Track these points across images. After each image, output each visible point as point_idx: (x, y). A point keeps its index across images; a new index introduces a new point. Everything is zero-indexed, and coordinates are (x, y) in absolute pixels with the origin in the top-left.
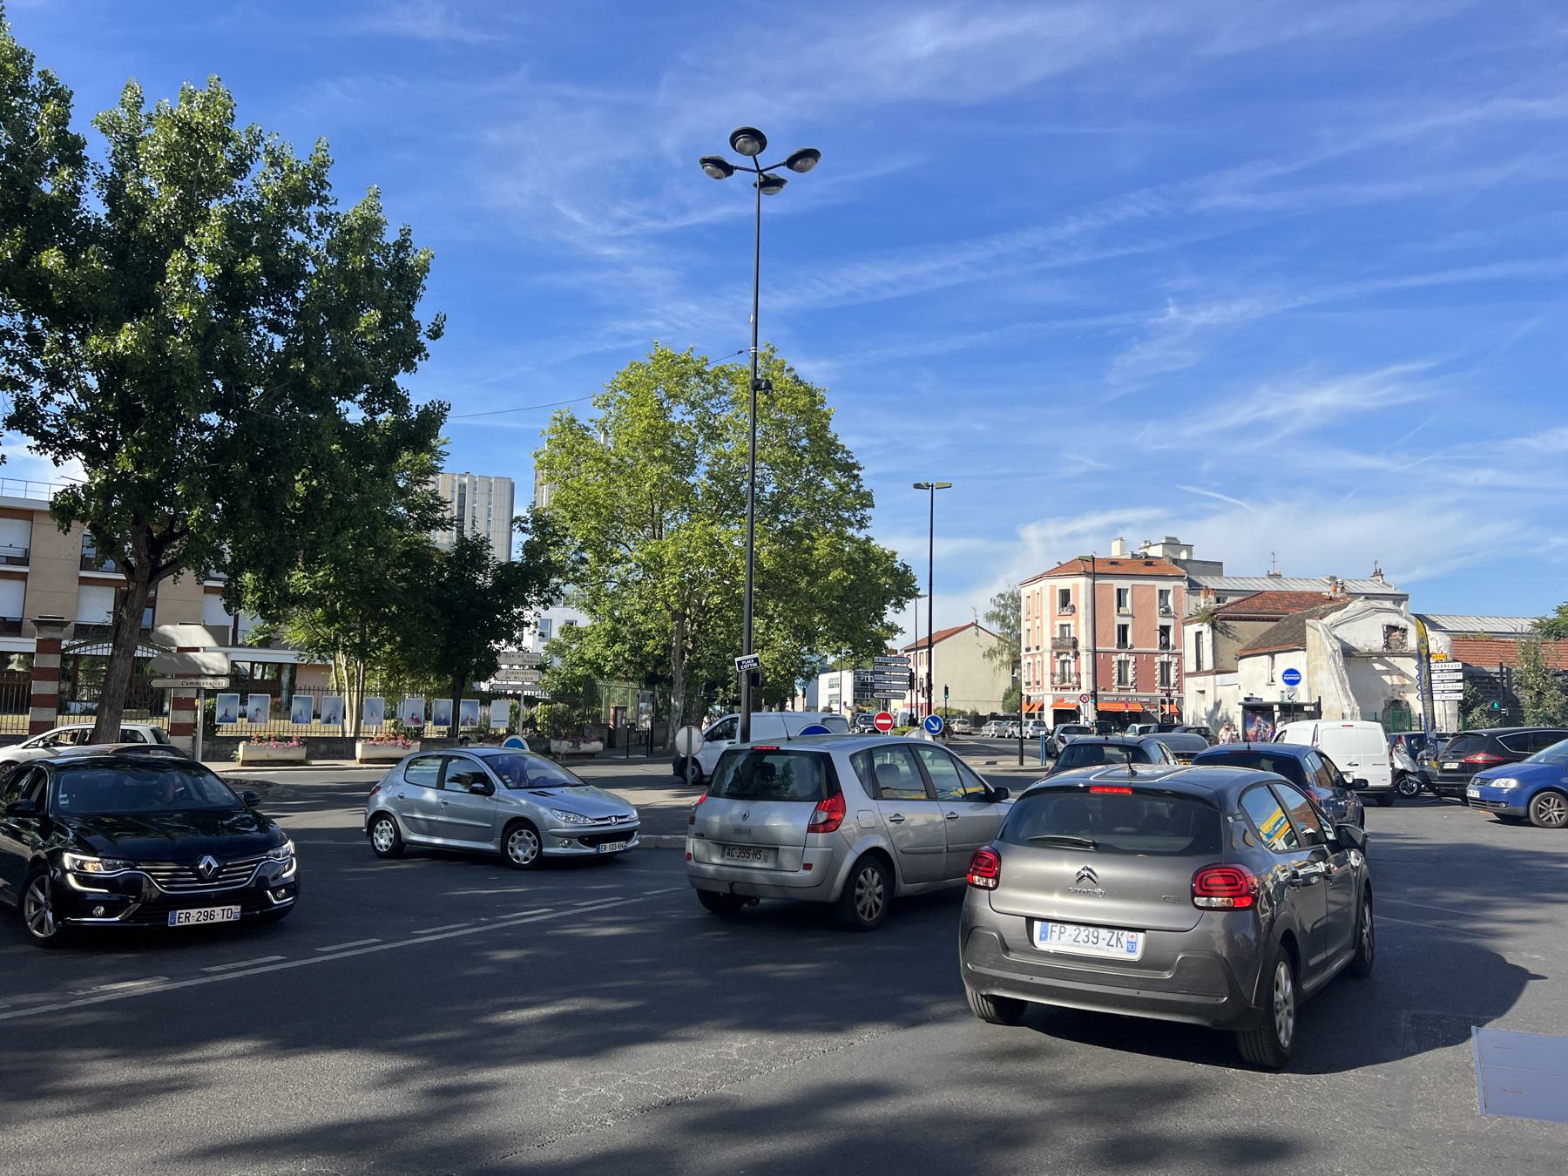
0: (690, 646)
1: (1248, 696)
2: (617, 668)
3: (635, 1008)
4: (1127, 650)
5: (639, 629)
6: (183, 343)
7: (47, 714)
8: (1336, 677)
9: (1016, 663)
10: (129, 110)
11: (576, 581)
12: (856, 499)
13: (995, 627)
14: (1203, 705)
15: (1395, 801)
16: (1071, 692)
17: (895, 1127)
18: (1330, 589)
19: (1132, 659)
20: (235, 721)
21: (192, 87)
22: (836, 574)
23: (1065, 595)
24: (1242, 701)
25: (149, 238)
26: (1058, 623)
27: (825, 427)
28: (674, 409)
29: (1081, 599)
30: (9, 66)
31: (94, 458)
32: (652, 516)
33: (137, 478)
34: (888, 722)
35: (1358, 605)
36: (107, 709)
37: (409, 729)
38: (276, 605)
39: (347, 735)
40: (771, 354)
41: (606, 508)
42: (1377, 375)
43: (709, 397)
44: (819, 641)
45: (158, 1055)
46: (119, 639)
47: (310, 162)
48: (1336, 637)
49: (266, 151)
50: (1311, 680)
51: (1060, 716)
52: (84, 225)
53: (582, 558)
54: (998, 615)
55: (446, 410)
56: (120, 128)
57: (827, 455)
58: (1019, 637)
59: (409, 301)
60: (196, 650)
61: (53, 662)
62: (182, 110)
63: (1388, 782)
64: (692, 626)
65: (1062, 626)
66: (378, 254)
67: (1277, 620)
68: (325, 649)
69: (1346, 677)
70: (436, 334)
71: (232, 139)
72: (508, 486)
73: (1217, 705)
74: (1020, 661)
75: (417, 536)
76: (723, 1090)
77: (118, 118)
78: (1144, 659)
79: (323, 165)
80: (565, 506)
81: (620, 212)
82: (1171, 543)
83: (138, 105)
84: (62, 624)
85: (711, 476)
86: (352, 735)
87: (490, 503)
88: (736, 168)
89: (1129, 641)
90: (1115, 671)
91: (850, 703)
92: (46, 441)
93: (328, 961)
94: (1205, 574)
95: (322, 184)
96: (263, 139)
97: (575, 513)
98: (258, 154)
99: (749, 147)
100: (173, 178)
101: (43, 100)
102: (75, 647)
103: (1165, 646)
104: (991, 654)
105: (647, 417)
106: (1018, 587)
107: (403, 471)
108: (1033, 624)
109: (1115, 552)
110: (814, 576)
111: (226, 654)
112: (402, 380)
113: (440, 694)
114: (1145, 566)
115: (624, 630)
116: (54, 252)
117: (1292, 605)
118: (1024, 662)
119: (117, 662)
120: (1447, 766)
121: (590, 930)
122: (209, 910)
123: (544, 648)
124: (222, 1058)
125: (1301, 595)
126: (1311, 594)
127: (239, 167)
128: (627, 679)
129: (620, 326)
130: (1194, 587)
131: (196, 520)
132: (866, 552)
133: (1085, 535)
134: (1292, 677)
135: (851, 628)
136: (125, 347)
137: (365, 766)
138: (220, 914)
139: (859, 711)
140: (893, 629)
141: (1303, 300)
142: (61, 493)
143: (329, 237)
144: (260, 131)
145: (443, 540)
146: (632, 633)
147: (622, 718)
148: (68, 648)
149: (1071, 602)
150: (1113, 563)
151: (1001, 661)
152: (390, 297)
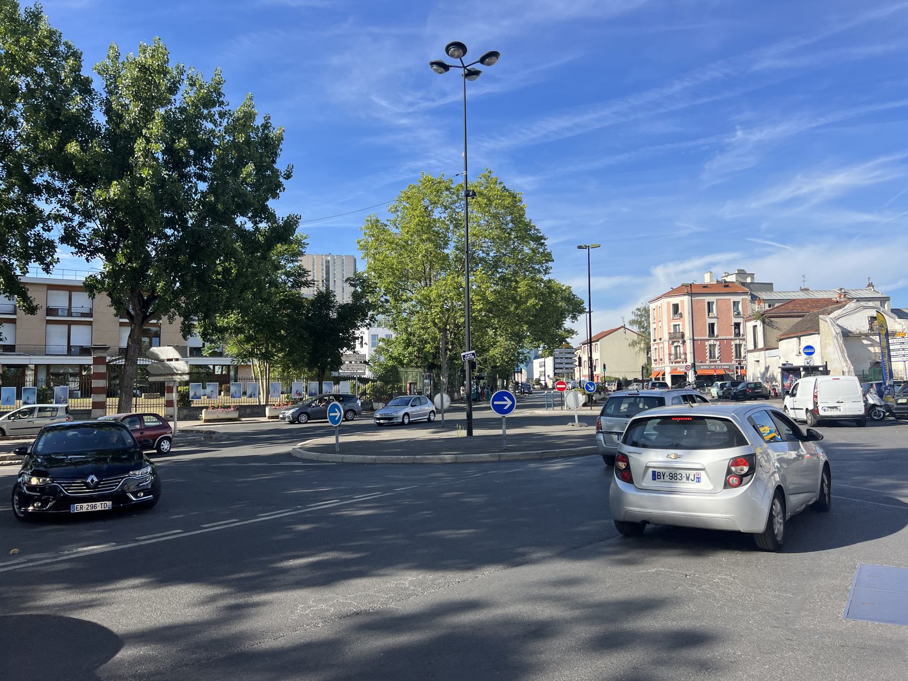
0: (450, 347)
1: (785, 363)
2: (411, 361)
3: (362, 558)
4: (714, 338)
5: (423, 338)
6: (146, 191)
7: (101, 398)
8: (838, 349)
9: (648, 349)
10: (112, 61)
11: (383, 313)
12: (542, 257)
13: (635, 328)
14: (759, 369)
15: (867, 423)
16: (681, 364)
17: (481, 626)
18: (837, 296)
19: (718, 343)
20: (200, 398)
21: (145, 44)
22: (532, 301)
23: (676, 307)
24: (781, 366)
25: (125, 131)
26: (672, 324)
27: (522, 216)
28: (435, 210)
29: (685, 309)
30: (46, 41)
31: (110, 257)
32: (424, 273)
33: (129, 267)
34: (564, 386)
35: (852, 305)
36: (124, 394)
37: (295, 399)
38: (211, 332)
39: (262, 404)
40: (489, 174)
41: (398, 270)
42: (871, 164)
43: (454, 202)
44: (526, 341)
45: (92, 587)
46: (128, 357)
47: (211, 82)
48: (838, 325)
49: (188, 78)
50: (823, 352)
51: (675, 378)
52: (91, 127)
53: (386, 300)
54: (637, 321)
55: (298, 219)
56: (108, 71)
57: (526, 232)
58: (649, 334)
59: (273, 158)
60: (171, 360)
61: (102, 369)
62: (141, 58)
63: (862, 412)
64: (451, 335)
65: (675, 326)
66: (252, 132)
67: (803, 316)
68: (245, 356)
69: (844, 349)
70: (288, 176)
71: (168, 72)
72: (352, 260)
73: (767, 369)
74: (650, 348)
75: (294, 291)
76: (392, 605)
77: (107, 65)
78: (727, 342)
79: (219, 83)
80: (374, 270)
81: (408, 99)
82: (741, 273)
83: (117, 57)
84: (105, 349)
85: (457, 248)
86: (264, 404)
87: (343, 271)
88: (451, 66)
89: (716, 333)
90: (708, 351)
91: (552, 375)
92: (81, 249)
93: (205, 532)
94: (762, 290)
95: (220, 94)
96: (185, 71)
97: (380, 274)
98: (183, 80)
99: (457, 53)
100: (137, 97)
101: (66, 58)
102: (113, 360)
103: (738, 334)
104: (633, 344)
105: (418, 216)
106: (648, 304)
107: (283, 255)
108: (657, 325)
109: (707, 279)
110: (519, 303)
111: (187, 362)
112: (271, 204)
113: (312, 379)
114: (725, 287)
115: (415, 339)
116: (74, 143)
117: (813, 307)
118: (652, 348)
119: (128, 368)
120: (900, 401)
121: (355, 512)
122: (94, 504)
123: (374, 351)
124: (125, 588)
125: (818, 300)
126: (824, 300)
127: (173, 90)
128: (417, 367)
129: (412, 164)
130: (754, 298)
131: (161, 288)
132: (549, 288)
133: (692, 271)
134: (809, 351)
135: (542, 333)
136: (114, 195)
137: (271, 420)
138: (99, 506)
139: (557, 380)
140: (571, 332)
141: (822, 121)
142: (89, 277)
143: (226, 124)
144: (183, 67)
145: (308, 293)
146: (419, 341)
147: (414, 389)
148: (110, 361)
149: (680, 311)
150: (704, 287)
151: (640, 348)
152: (262, 157)
